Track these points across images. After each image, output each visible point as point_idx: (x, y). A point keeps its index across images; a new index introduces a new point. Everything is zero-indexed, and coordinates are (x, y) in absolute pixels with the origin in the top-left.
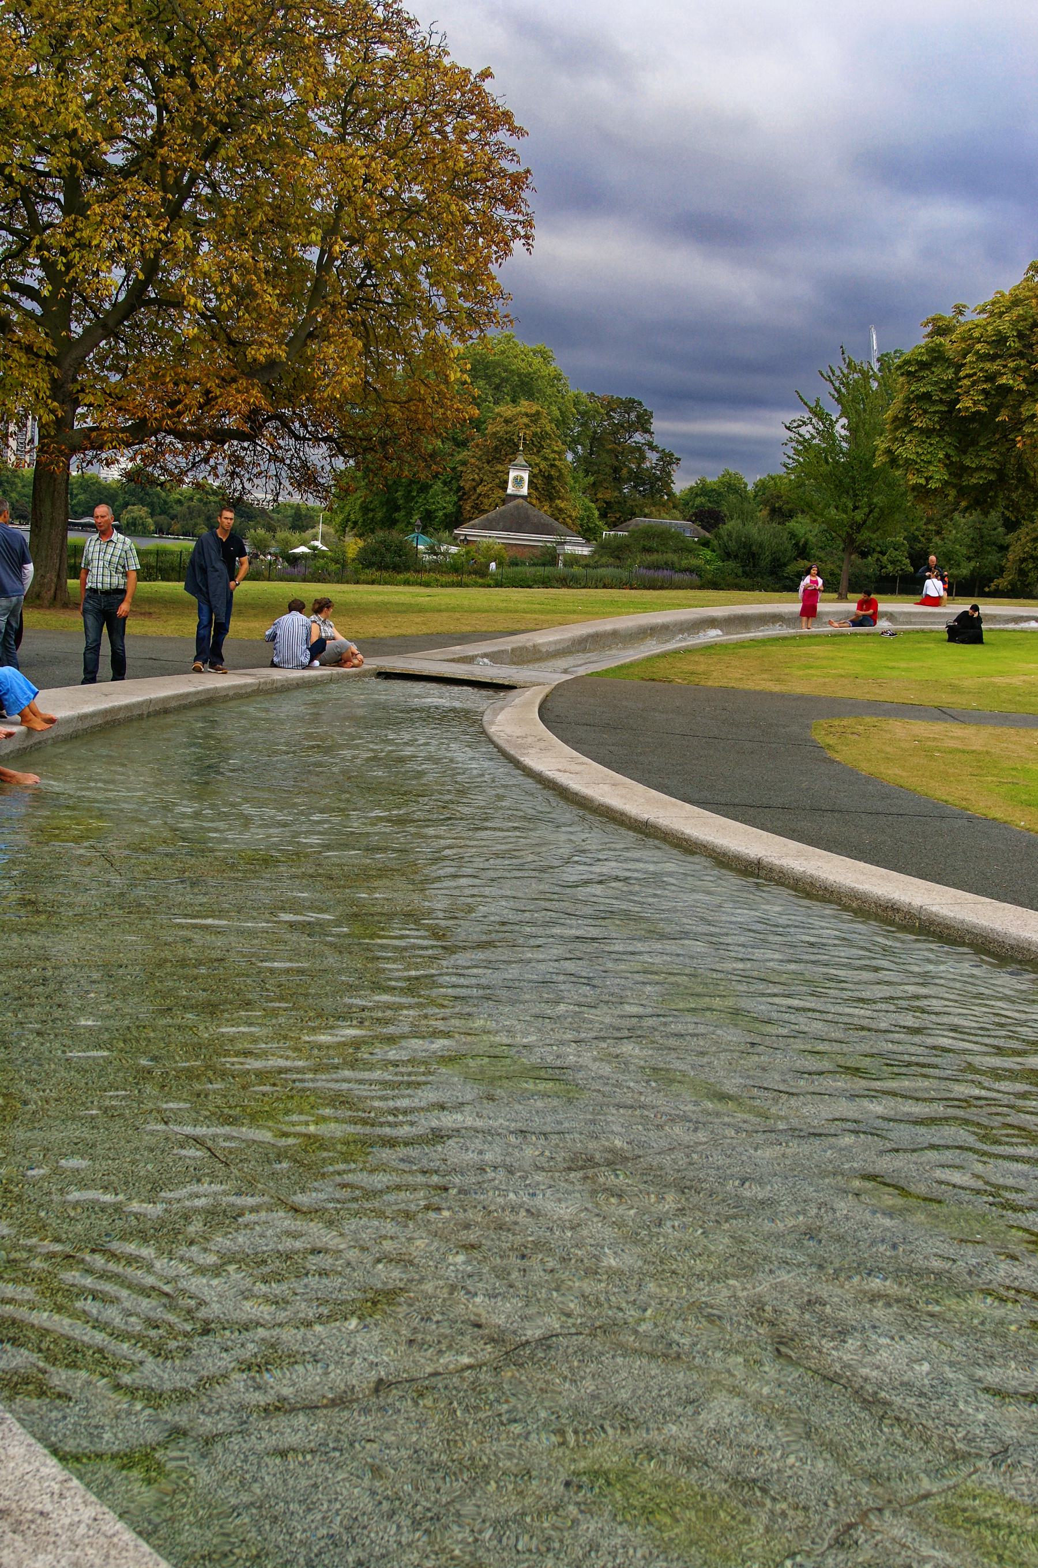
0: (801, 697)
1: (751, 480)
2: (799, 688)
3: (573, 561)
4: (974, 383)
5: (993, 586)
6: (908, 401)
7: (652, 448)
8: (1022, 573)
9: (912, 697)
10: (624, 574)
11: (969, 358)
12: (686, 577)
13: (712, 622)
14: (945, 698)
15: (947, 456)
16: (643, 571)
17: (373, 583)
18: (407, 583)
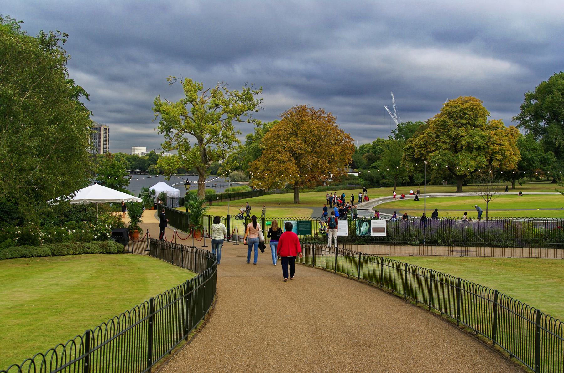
8: (435, 181)
13: (380, 200)
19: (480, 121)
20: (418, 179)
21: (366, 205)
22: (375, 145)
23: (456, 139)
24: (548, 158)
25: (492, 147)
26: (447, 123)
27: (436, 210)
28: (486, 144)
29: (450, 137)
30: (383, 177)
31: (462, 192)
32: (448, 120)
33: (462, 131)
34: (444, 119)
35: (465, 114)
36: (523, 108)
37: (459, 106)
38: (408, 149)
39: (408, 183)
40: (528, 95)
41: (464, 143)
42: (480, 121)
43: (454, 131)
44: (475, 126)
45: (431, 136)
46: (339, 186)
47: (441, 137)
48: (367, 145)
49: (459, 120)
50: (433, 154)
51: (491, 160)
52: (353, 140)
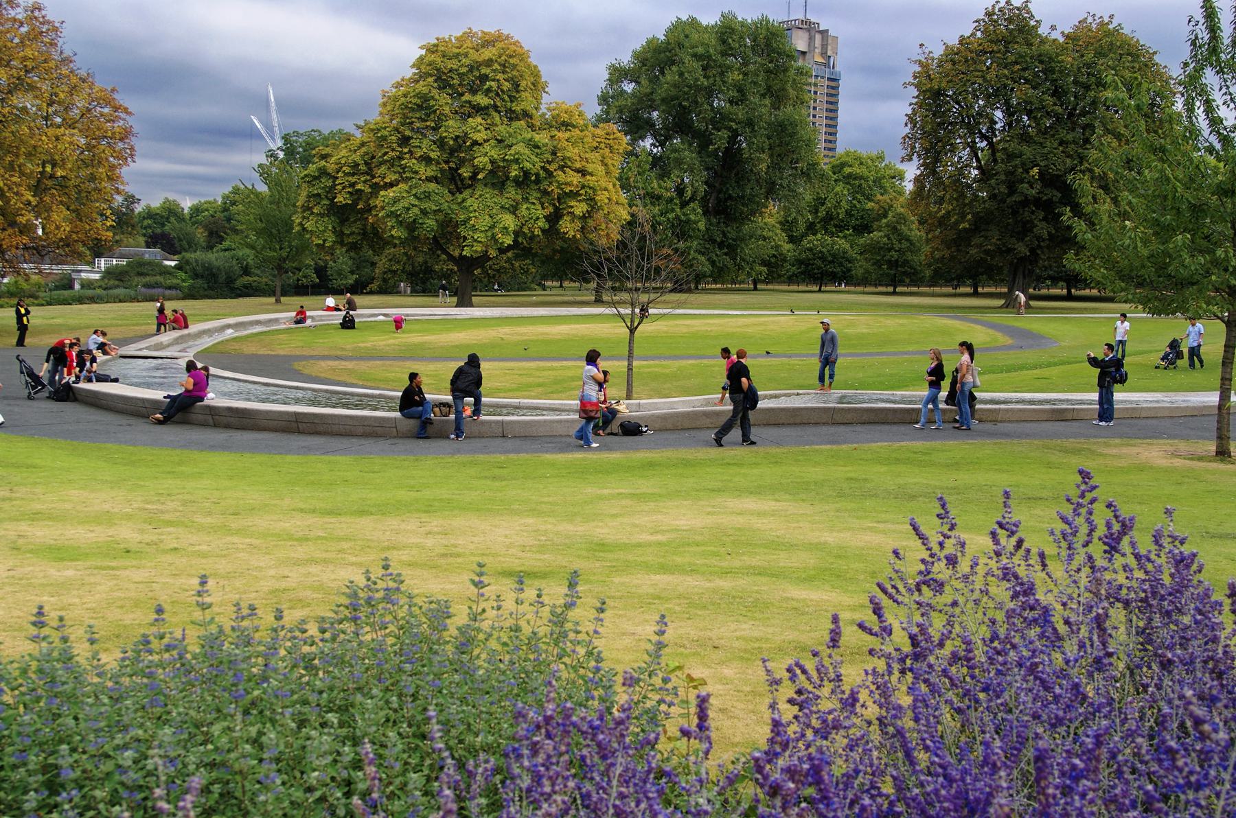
1: (187, 204)
2: (282, 353)
3: (87, 285)
6: (309, 197)
7: (119, 193)
8: (385, 280)
9: (326, 353)
11: (340, 174)
12: (174, 292)
13: (229, 326)
14: (339, 353)
16: (143, 290)
19: (526, 102)
20: (339, 273)
21: (176, 341)
22: (229, 202)
23: (458, 149)
24: (688, 221)
25: (560, 176)
26: (432, 103)
27: (473, 361)
28: (542, 168)
29: (441, 143)
30: (246, 271)
31: (471, 306)
32: (435, 92)
34: (425, 90)
35: (484, 78)
36: (604, 99)
37: (466, 55)
38: (315, 178)
39: (314, 286)
41: (481, 161)
42: (526, 102)
43: (452, 127)
44: (512, 116)
45: (384, 138)
48: (209, 202)
50: (391, 193)
51: (554, 218)
52: (126, 110)
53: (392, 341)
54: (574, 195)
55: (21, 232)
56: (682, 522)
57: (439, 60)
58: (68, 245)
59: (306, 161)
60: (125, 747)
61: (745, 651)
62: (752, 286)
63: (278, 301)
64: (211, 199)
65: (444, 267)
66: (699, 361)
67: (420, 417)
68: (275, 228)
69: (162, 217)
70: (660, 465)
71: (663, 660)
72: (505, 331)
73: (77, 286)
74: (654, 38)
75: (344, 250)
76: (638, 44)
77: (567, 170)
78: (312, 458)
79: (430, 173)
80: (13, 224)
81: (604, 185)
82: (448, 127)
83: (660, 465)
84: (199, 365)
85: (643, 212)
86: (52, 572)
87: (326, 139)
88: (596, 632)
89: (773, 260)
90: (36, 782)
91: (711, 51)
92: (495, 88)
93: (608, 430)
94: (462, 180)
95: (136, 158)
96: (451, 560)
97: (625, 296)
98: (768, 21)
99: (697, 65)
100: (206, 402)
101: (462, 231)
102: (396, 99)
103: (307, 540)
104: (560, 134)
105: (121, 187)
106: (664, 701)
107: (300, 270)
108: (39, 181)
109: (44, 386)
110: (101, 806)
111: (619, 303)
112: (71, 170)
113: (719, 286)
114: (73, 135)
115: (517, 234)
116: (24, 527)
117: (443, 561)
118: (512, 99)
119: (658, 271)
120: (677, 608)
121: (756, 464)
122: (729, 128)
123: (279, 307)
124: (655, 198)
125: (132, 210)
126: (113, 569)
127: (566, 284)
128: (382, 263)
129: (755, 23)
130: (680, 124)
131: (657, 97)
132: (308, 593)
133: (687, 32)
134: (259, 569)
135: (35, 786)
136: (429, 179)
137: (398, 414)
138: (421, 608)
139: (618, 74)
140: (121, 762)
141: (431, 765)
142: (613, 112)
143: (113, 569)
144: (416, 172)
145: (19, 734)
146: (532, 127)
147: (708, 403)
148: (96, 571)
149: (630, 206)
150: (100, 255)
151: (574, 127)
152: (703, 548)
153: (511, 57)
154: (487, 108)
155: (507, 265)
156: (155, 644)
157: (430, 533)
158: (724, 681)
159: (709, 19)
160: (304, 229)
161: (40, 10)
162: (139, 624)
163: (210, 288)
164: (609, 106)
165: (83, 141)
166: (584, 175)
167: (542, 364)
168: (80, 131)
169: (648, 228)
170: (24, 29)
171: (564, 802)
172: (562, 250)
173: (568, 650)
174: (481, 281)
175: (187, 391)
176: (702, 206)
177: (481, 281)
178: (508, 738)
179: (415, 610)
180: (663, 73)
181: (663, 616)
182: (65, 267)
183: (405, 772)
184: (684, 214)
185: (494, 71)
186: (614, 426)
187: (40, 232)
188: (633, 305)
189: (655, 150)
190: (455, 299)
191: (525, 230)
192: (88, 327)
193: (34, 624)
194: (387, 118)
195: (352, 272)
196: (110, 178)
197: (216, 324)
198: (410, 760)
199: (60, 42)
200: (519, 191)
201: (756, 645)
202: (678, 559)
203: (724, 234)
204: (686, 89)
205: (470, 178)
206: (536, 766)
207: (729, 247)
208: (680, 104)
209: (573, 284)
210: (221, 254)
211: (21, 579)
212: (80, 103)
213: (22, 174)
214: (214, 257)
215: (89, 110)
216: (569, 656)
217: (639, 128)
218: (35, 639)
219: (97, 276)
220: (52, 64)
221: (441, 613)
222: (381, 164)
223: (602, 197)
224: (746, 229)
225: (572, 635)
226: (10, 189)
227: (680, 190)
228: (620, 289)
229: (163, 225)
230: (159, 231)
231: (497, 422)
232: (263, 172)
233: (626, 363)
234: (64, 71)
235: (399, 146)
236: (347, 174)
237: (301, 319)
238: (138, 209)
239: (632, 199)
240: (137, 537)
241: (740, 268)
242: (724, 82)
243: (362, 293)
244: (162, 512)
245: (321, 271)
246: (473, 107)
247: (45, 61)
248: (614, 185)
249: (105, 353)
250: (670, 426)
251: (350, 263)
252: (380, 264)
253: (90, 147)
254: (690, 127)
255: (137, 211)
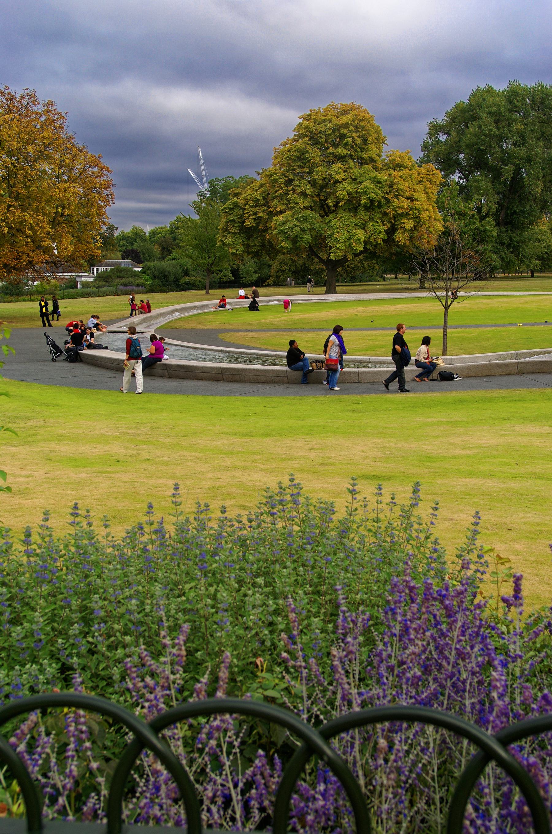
0: (212, 330)
1: (147, 229)
2: (211, 328)
3: (86, 285)
4: (250, 216)
5: (266, 283)
6: (227, 222)
7: (104, 223)
8: (277, 277)
9: (240, 327)
10: (114, 289)
12: (140, 288)
13: (177, 310)
14: (248, 327)
15: (243, 242)
16: (121, 287)
17: (11, 302)
18: (24, 301)
19: (372, 151)
20: (247, 273)
22: (174, 228)
23: (325, 187)
24: (485, 230)
25: (395, 202)
26: (307, 155)
29: (313, 183)
31: (335, 293)
33: (337, 170)
35: (343, 136)
36: (425, 147)
37: (330, 121)
38: (231, 209)
40: (434, 126)
42: (372, 151)
43: (321, 171)
44: (362, 162)
45: (275, 181)
46: (104, 289)
47: (297, 183)
48: (162, 228)
49: (331, 150)
50: (281, 218)
51: (391, 232)
53: (283, 318)
54: (405, 215)
55: (44, 252)
56: (483, 441)
57: (311, 125)
58: (73, 260)
59: (224, 199)
60: (130, 597)
61: (530, 532)
62: (530, 275)
63: (207, 293)
64: (163, 226)
65: (319, 267)
66: (492, 328)
67: (302, 370)
68: (205, 244)
69: (132, 239)
70: (467, 401)
71: (478, 543)
72: (359, 310)
73: (80, 286)
74: (461, 102)
75: (250, 257)
76: (450, 107)
77: (400, 197)
78: (233, 398)
79: (307, 204)
80: (39, 247)
81: (426, 207)
82: (318, 172)
83: (467, 401)
84: (158, 337)
85: (453, 226)
86: (72, 474)
87: (237, 182)
88: (432, 523)
89: (545, 256)
90: (76, 618)
91: (502, 109)
92: (351, 142)
93: (431, 377)
94: (329, 207)
95: (115, 201)
96: (327, 467)
97: (442, 284)
98: (542, 86)
99: (491, 119)
100: (163, 362)
101: (330, 243)
102: (283, 153)
103: (231, 453)
104: (395, 173)
105: (106, 220)
106: (479, 571)
107: (221, 271)
108: (54, 218)
109: (61, 352)
110: (118, 634)
111: (436, 288)
112: (74, 210)
113: (507, 275)
114: (75, 187)
115: (366, 243)
116: (53, 445)
117: (321, 468)
118: (362, 149)
119: (464, 266)
120: (481, 502)
121: (535, 401)
122: (514, 164)
123: (208, 296)
124: (461, 215)
125: (113, 235)
126: (110, 473)
127: (400, 276)
128: (276, 265)
129: (533, 88)
130: (479, 163)
131: (463, 144)
132: (234, 489)
133: (484, 97)
134: (202, 473)
135: (76, 620)
136: (306, 208)
137: (286, 368)
138: (315, 506)
139: (435, 129)
140: (130, 607)
141: (325, 612)
142: (432, 156)
143: (110, 473)
144: (298, 203)
145: (65, 587)
146: (376, 169)
147: (500, 357)
148: (99, 474)
149: (444, 221)
150: (93, 266)
151: (405, 167)
152: (498, 460)
153: (361, 120)
154: (345, 157)
155: (359, 264)
156: (147, 529)
157: (312, 449)
158: (516, 553)
159: (501, 87)
160: (224, 244)
161: (52, 105)
162: (128, 510)
163: (164, 285)
164: (429, 151)
165: (81, 191)
166: (412, 201)
167: (383, 332)
168: (79, 184)
169: (457, 237)
170: (43, 119)
171: (423, 645)
172: (397, 254)
173: (414, 536)
174: (341, 276)
175: (151, 354)
176: (495, 219)
177: (341, 276)
178: (376, 597)
179: (311, 508)
180: (467, 127)
181: (477, 513)
182: (72, 274)
183: (308, 617)
184: (483, 226)
185: (350, 131)
186: (435, 375)
187: (55, 251)
188: (447, 291)
189: (461, 181)
190: (324, 289)
191: (372, 240)
192: (87, 313)
193: (72, 514)
194: (278, 167)
195: (256, 272)
196: (99, 215)
197: (169, 309)
198: (311, 609)
199: (65, 126)
200: (368, 213)
201: (538, 528)
202: (481, 467)
203: (511, 238)
204: (483, 137)
205: (334, 206)
206: (406, 620)
207: (514, 247)
208: (479, 149)
209: (404, 276)
210: (170, 262)
211: (53, 479)
212: (79, 166)
213: (44, 214)
214: (166, 264)
215: (84, 170)
216: (414, 540)
217: (450, 166)
218: (73, 524)
219: (92, 279)
220: (61, 141)
221: (329, 509)
222: (274, 198)
223: (425, 216)
224: (526, 234)
225: (416, 526)
226: (37, 225)
227: (479, 210)
228: (438, 279)
229: (133, 244)
230: (130, 248)
231: (355, 372)
232: (197, 206)
233: (442, 331)
234: (69, 145)
235: (286, 186)
236: (251, 207)
237: (223, 304)
238: (117, 234)
239: (445, 217)
240: (124, 452)
241: (522, 262)
242: (510, 131)
243: (262, 286)
244: (138, 435)
245: (235, 272)
246: (336, 157)
247: (57, 139)
248: (433, 207)
249: (99, 330)
250: (473, 374)
251: (254, 266)
252: (274, 266)
253: (86, 195)
254: (486, 164)
255: (116, 236)
